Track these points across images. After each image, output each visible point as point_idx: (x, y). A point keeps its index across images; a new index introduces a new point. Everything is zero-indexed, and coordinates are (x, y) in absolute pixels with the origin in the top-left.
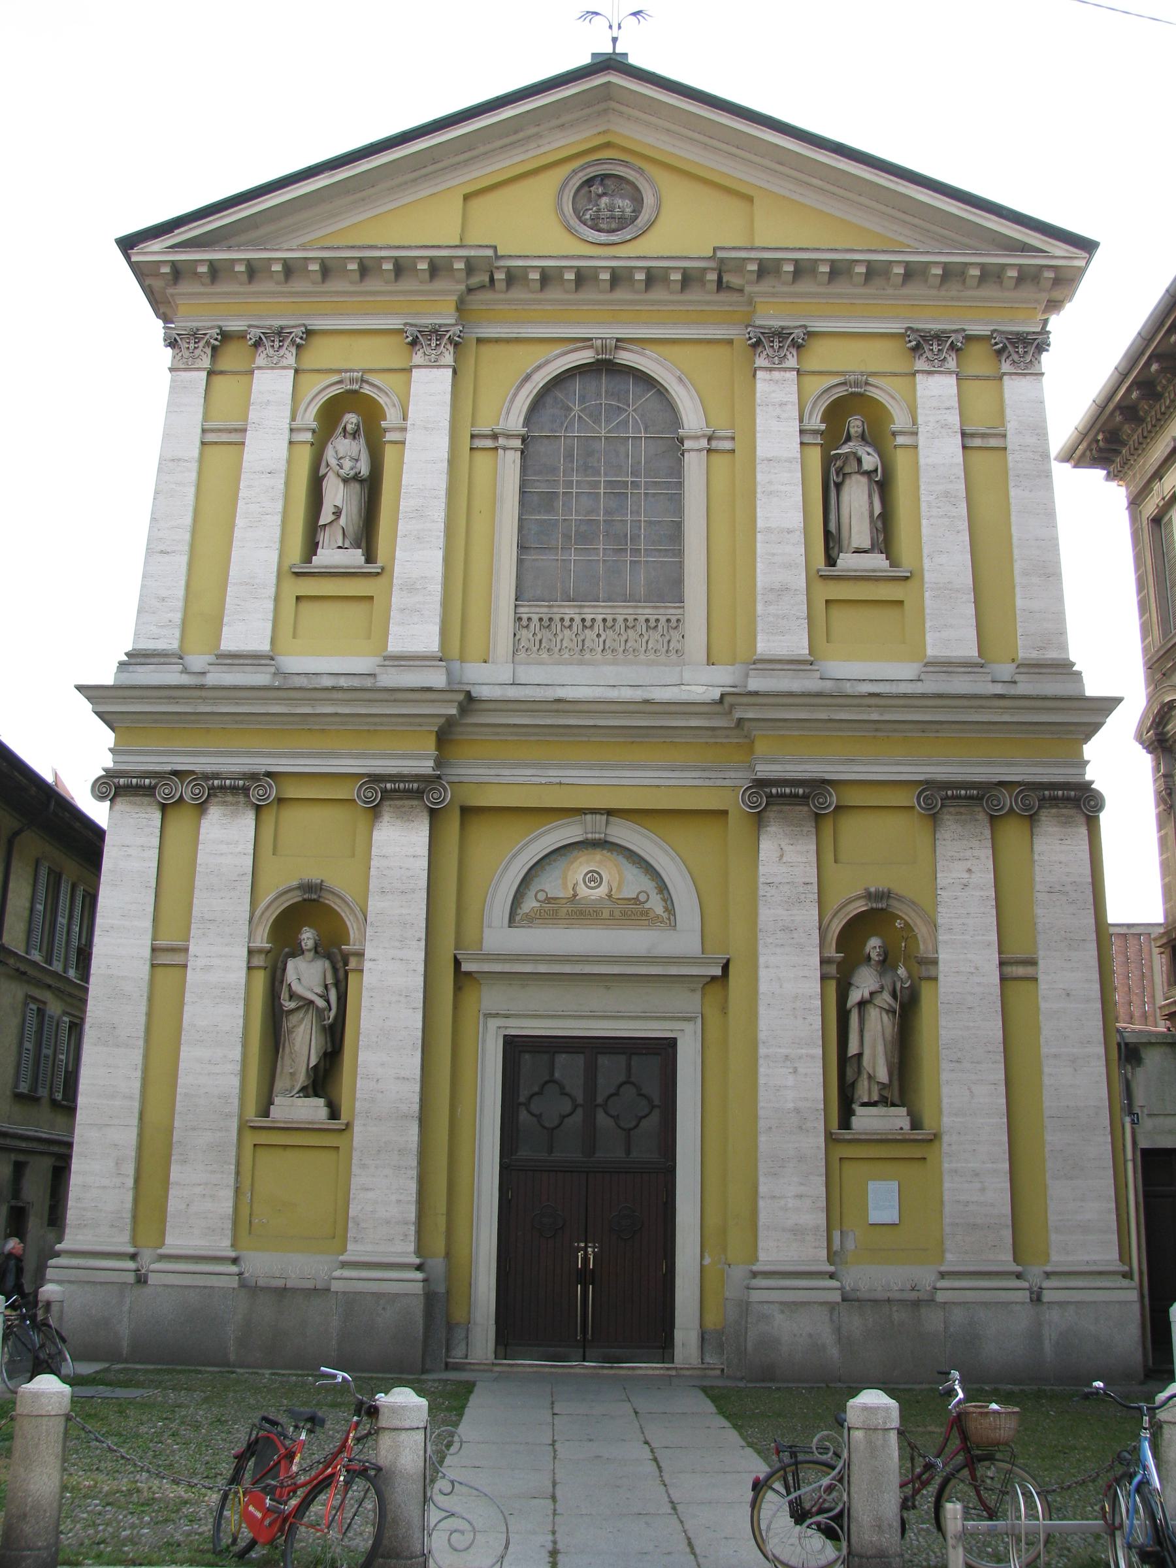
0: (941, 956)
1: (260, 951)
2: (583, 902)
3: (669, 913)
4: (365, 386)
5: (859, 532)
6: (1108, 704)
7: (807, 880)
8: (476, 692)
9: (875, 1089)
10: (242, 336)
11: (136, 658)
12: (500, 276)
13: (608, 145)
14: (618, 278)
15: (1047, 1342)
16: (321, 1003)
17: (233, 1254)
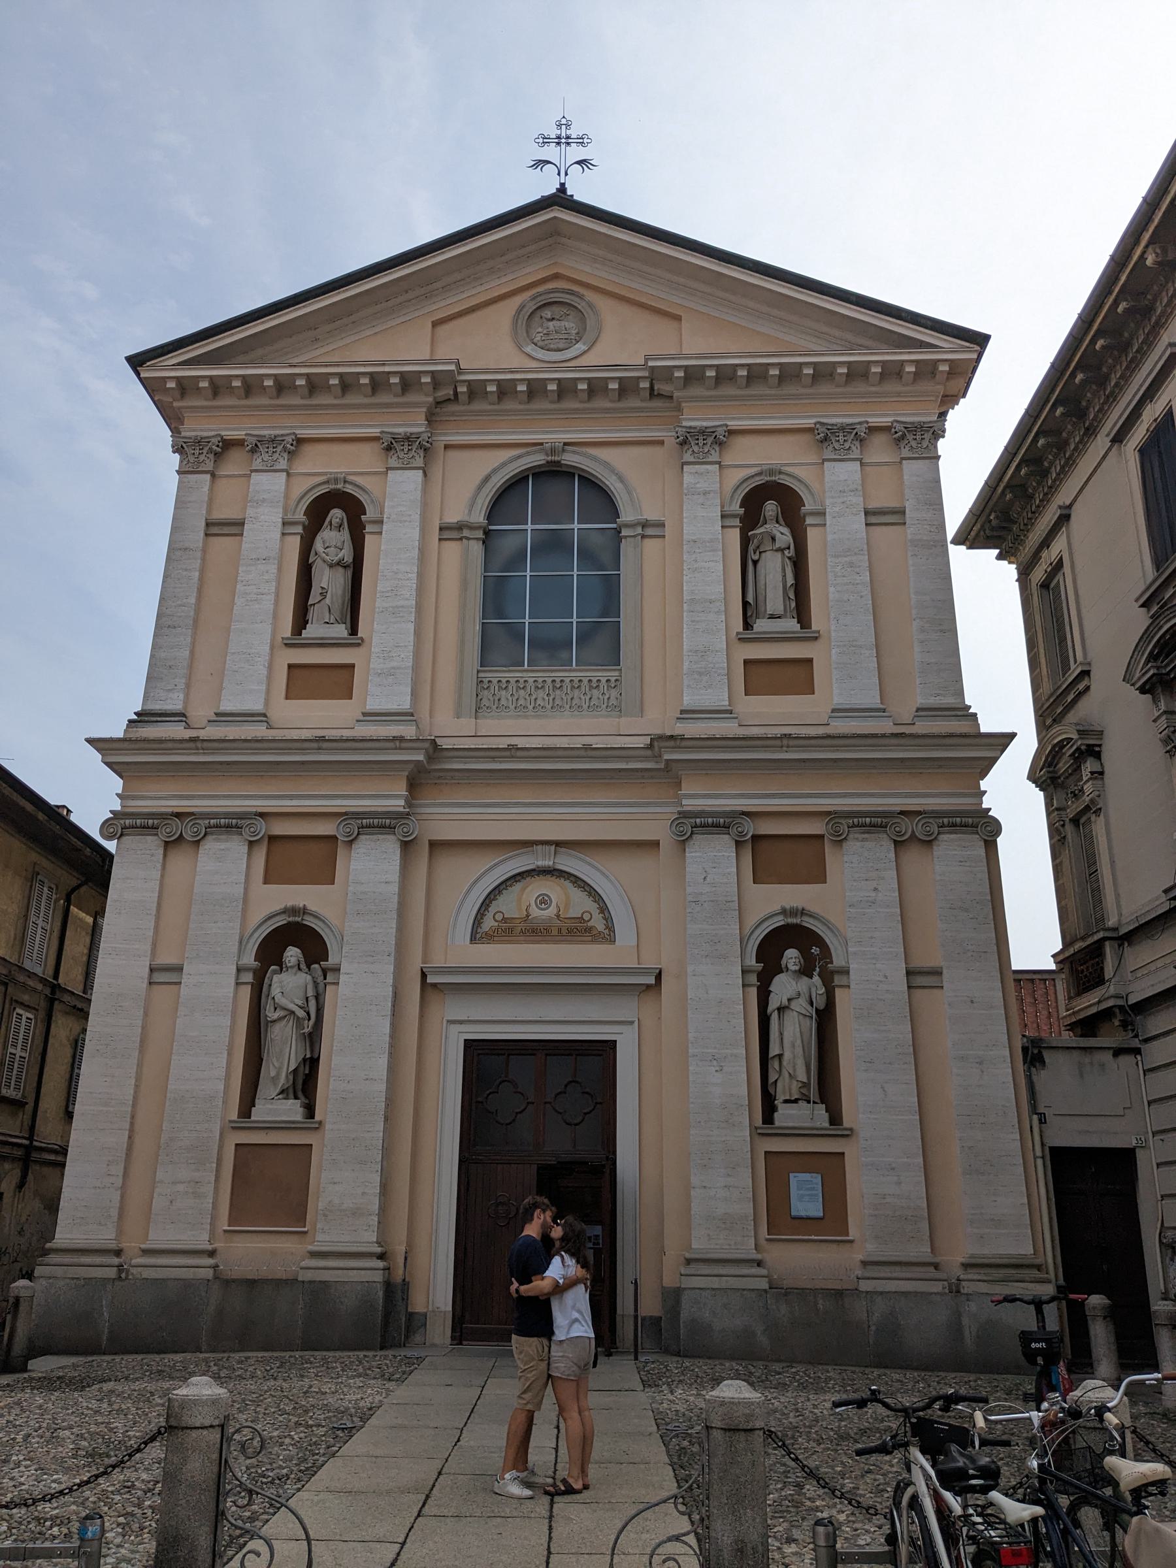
0: (851, 966)
1: (247, 969)
2: (535, 921)
3: (610, 930)
4: (347, 486)
5: (775, 600)
6: (1004, 740)
7: (729, 899)
8: (445, 744)
10: (240, 443)
11: (143, 717)
12: (462, 389)
13: (556, 276)
14: (565, 389)
15: (967, 1333)
16: (301, 1013)
17: (210, 1247)
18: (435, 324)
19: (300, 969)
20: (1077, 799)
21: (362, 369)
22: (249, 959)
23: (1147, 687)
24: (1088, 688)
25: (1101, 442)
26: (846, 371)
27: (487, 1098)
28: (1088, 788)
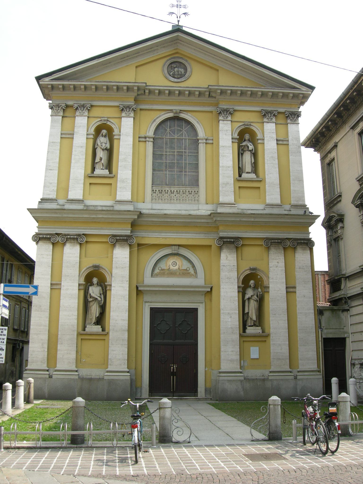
5: (248, 167)
9: (252, 322)
10: (72, 106)
11: (43, 200)
12: (147, 91)
14: (181, 93)
18: (136, 67)
19: (97, 285)
20: (336, 233)
21: (114, 84)
22: (82, 282)
23: (358, 206)
24: (340, 201)
25: (347, 128)
26: (271, 94)
27: (157, 325)
28: (339, 231)
